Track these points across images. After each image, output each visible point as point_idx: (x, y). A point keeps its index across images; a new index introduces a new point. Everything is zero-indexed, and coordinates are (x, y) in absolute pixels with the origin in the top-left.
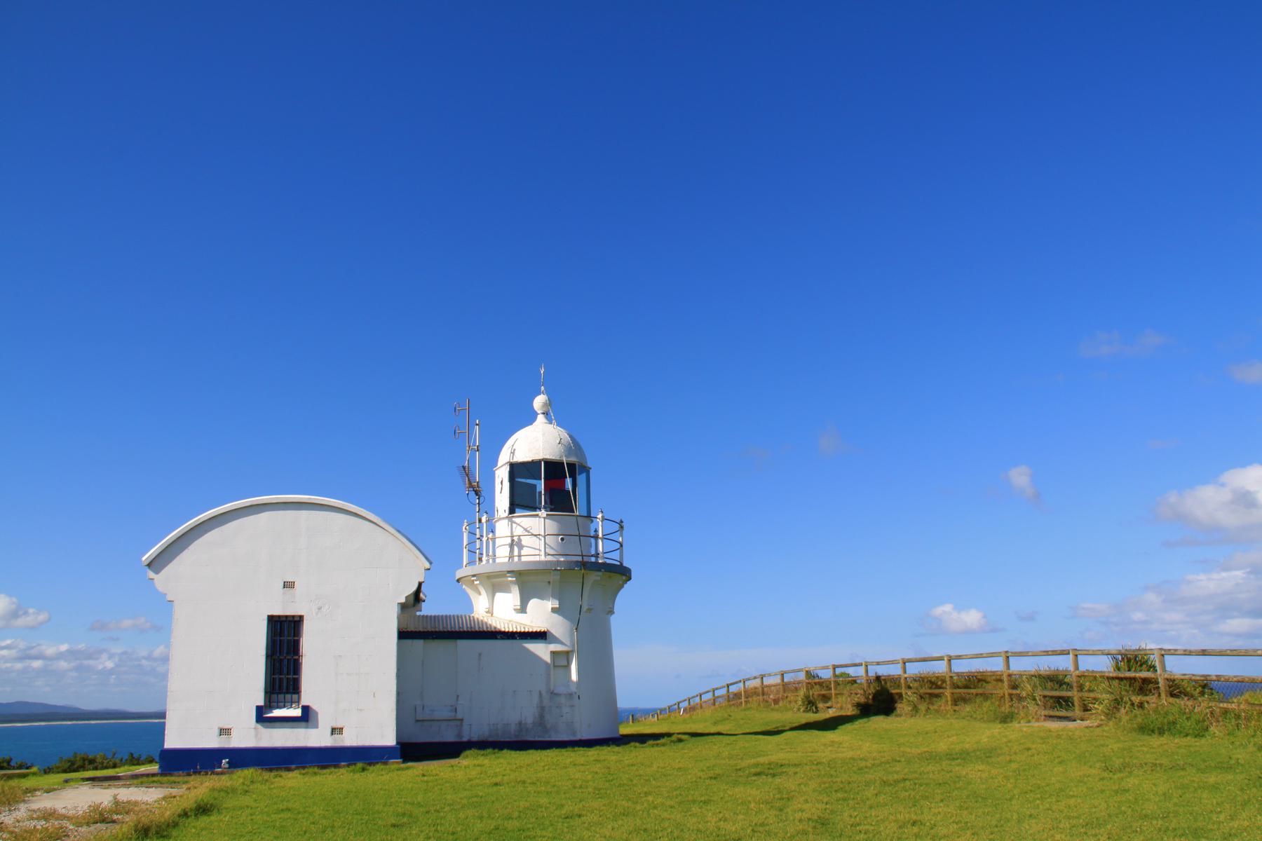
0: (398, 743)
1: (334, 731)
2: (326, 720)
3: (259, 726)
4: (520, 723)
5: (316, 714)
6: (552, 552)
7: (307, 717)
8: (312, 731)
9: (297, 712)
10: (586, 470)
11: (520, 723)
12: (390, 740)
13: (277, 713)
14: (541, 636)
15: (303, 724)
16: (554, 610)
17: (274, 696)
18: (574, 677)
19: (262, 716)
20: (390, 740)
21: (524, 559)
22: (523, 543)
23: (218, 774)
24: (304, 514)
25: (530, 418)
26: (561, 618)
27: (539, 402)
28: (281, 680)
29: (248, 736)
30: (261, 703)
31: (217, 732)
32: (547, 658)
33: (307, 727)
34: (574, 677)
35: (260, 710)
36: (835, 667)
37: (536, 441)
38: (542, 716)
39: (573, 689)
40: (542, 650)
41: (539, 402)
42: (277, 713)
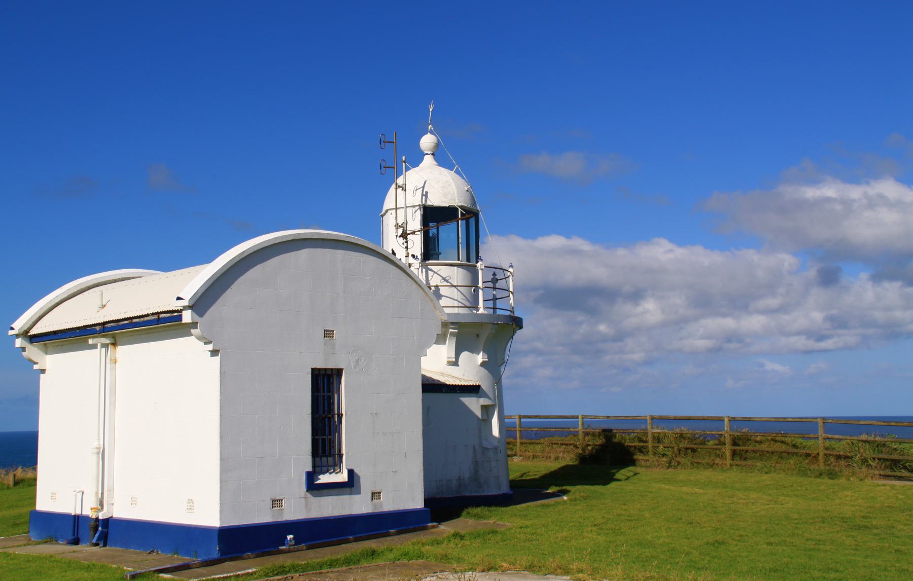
0: (427, 501)
1: (375, 495)
2: (366, 486)
3: (308, 495)
4: (459, 479)
5: (359, 477)
6: (468, 304)
7: (351, 484)
8: (356, 497)
9: (343, 477)
10: (476, 215)
11: (459, 479)
12: (418, 503)
13: (324, 479)
14: (474, 390)
15: (348, 489)
16: (483, 364)
17: (318, 459)
18: (496, 432)
19: (313, 487)
20: (418, 503)
21: (499, 312)
22: (442, 292)
23: (283, 552)
24: (340, 254)
25: (416, 159)
26: (486, 371)
27: (427, 141)
28: (324, 440)
29: (299, 507)
30: (310, 469)
31: (270, 503)
32: (478, 413)
33: (351, 494)
34: (496, 432)
35: (311, 477)
36: (521, 417)
37: (432, 182)
38: (476, 471)
39: (496, 444)
40: (474, 404)
41: (427, 141)
42: (324, 479)
